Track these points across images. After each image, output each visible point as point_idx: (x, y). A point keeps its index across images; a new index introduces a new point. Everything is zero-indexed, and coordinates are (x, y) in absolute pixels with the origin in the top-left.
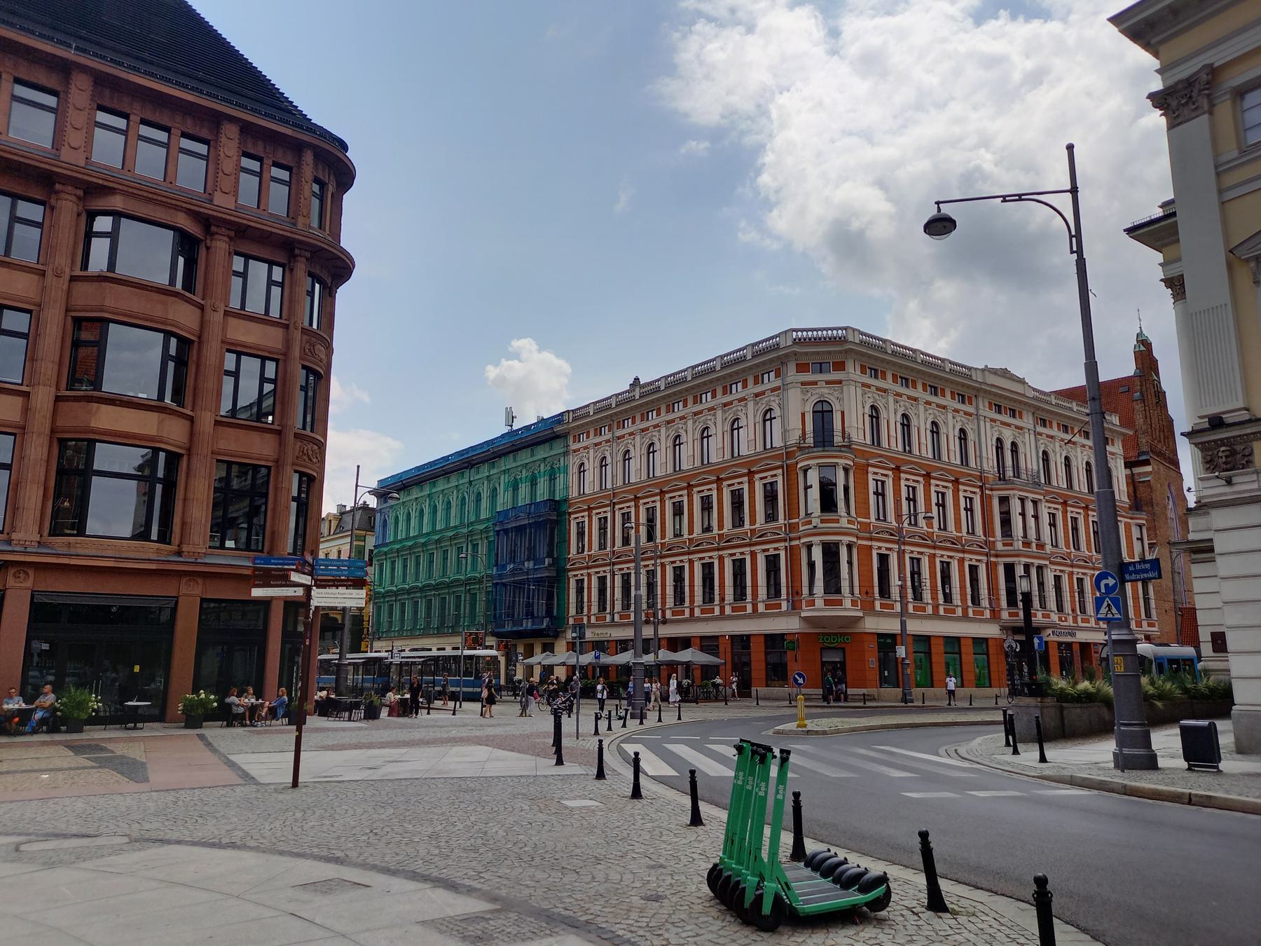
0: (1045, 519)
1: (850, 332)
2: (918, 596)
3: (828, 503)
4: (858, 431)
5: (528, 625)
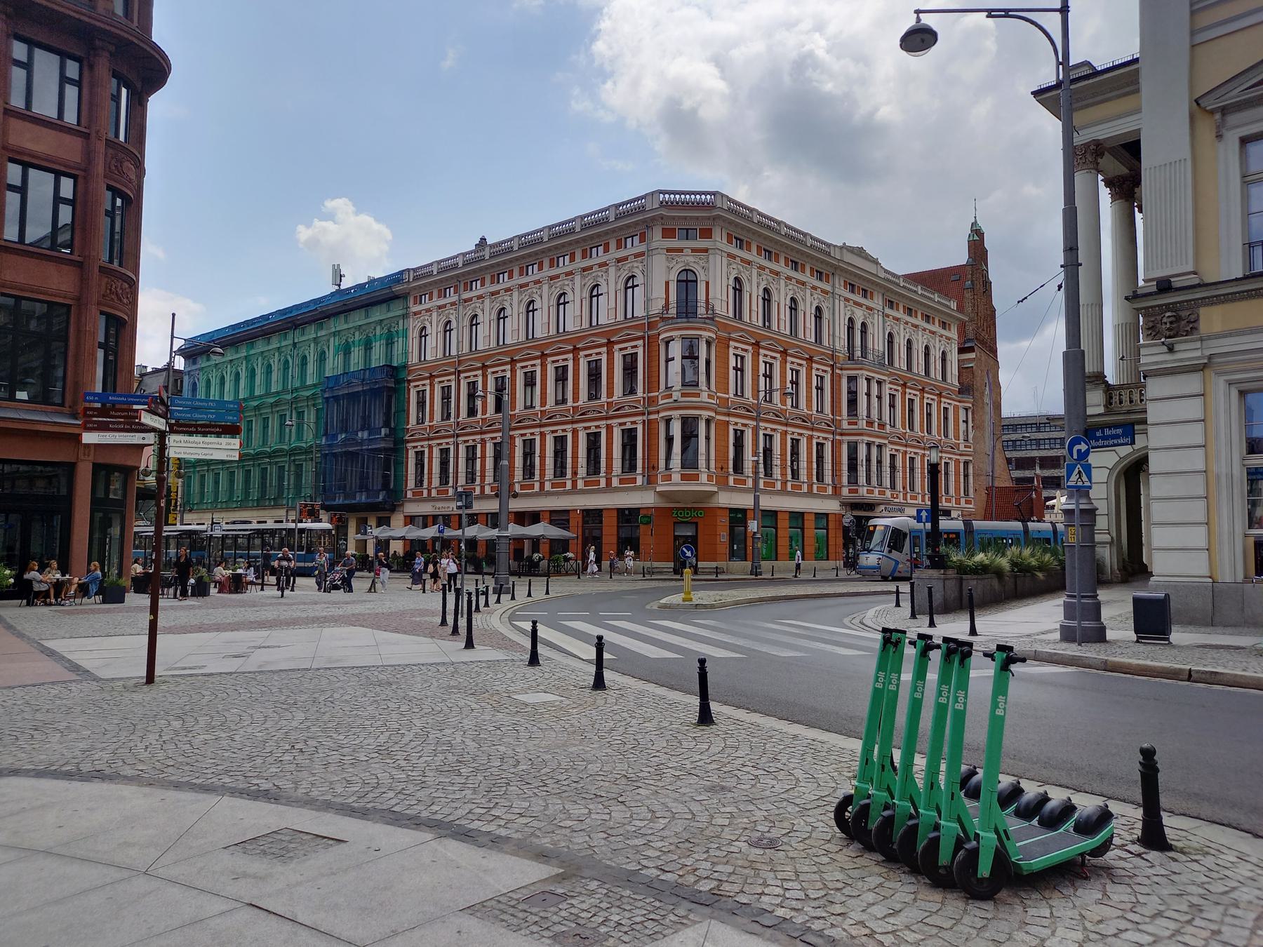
1: (719, 197)
2: (768, 473)
3: (690, 384)
4: (722, 302)
5: (362, 498)
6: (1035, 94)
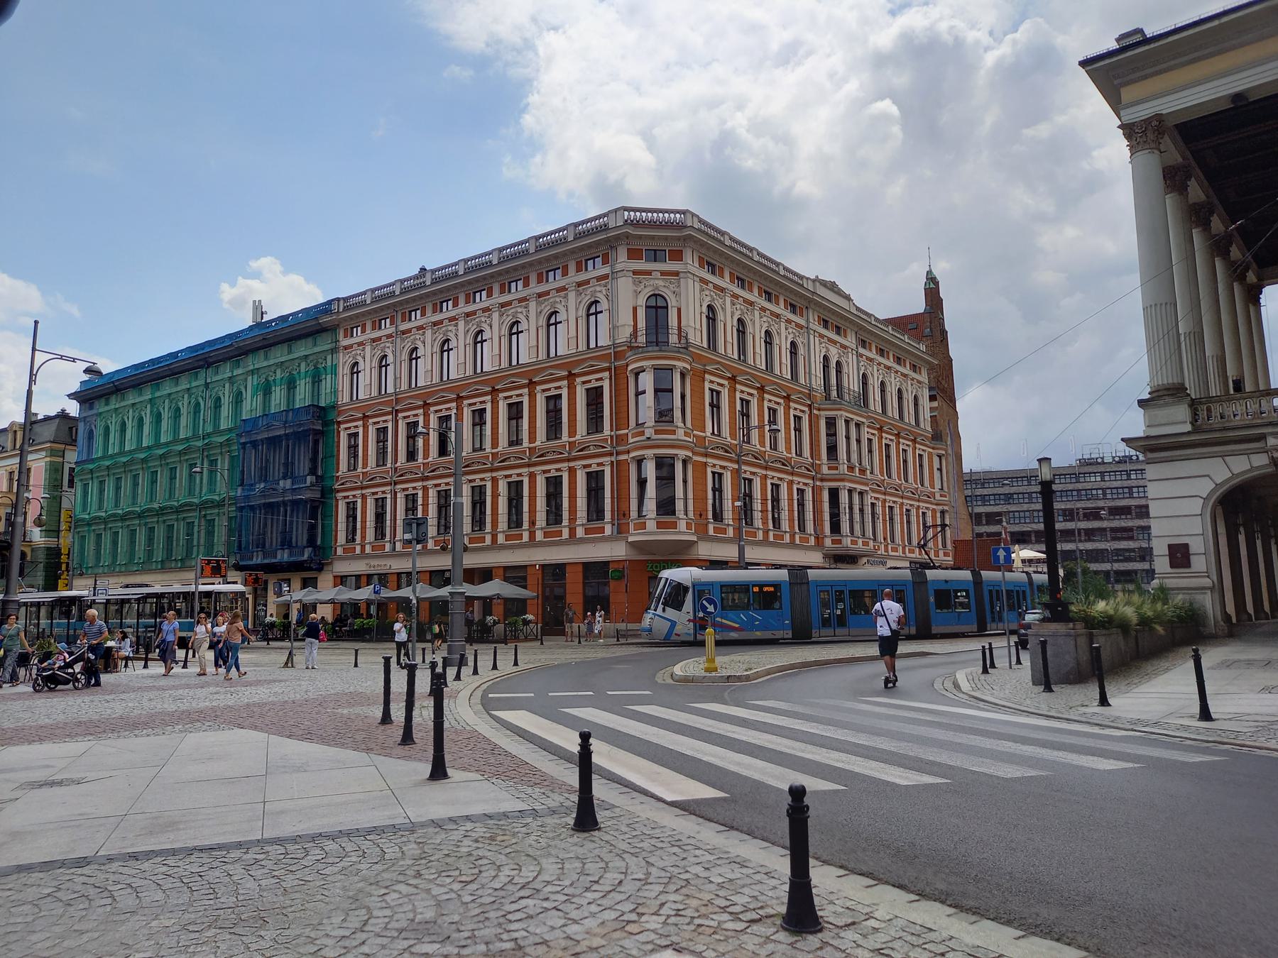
0: (865, 444)
1: (689, 216)
3: (664, 415)
5: (284, 556)
6: (1083, 64)
